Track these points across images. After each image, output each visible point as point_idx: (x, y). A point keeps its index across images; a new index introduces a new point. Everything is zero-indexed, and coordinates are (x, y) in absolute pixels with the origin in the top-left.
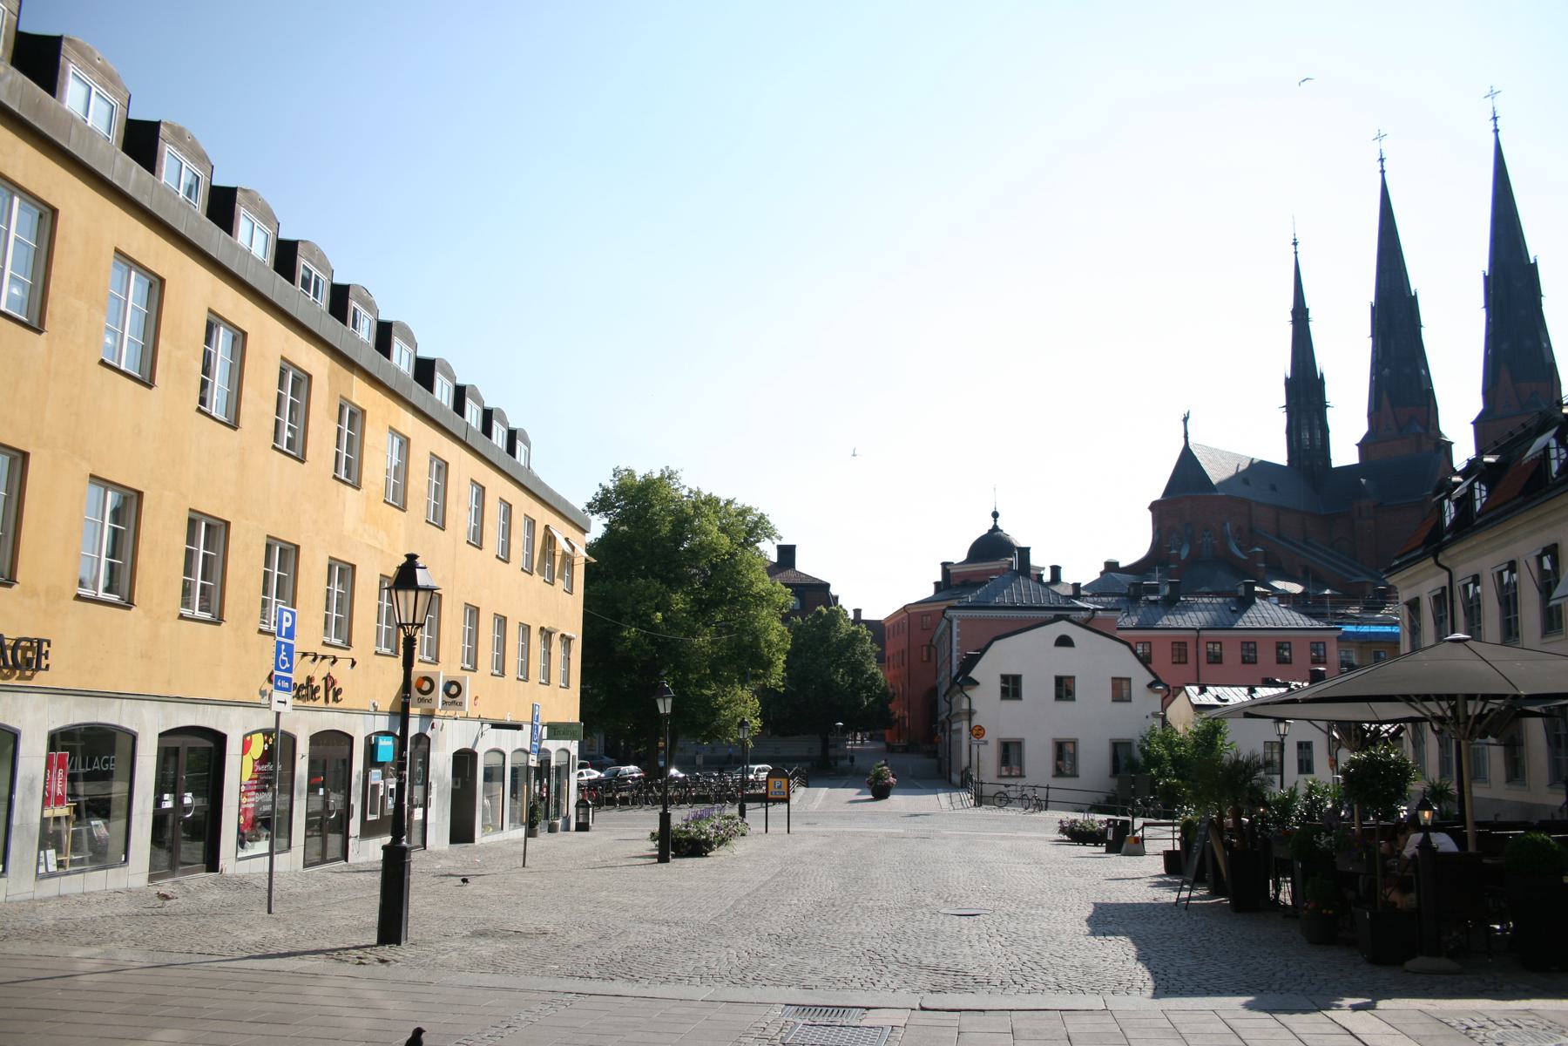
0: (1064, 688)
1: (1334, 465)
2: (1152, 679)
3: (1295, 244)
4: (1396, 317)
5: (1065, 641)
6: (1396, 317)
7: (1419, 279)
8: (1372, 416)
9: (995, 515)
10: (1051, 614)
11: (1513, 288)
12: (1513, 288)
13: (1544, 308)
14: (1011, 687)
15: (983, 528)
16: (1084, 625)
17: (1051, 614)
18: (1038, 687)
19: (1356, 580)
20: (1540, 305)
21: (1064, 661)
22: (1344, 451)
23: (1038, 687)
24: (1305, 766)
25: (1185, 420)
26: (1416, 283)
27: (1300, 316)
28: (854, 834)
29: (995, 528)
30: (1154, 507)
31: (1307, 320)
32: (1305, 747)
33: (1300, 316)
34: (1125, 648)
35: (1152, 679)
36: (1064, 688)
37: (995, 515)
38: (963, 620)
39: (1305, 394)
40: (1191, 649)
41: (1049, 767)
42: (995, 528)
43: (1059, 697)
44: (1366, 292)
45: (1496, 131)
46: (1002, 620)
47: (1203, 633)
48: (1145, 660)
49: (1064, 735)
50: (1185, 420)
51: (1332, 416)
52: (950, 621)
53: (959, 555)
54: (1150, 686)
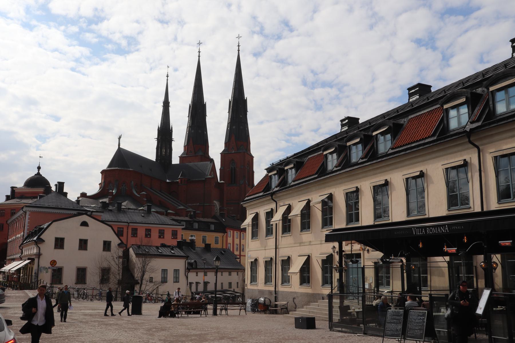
0: (83, 244)
1: (173, 163)
2: (120, 242)
3: (167, 76)
4: (198, 110)
5: (84, 224)
6: (198, 110)
7: (207, 98)
8: (226, 144)
9: (39, 168)
10: (75, 212)
11: (238, 106)
12: (238, 106)
13: (248, 116)
14: (59, 243)
15: (33, 173)
16: (90, 216)
17: (75, 212)
18: (71, 243)
19: (180, 208)
20: (247, 115)
21: (84, 233)
22: (175, 160)
23: (71, 243)
24: (176, 280)
25: (119, 138)
26: (246, 95)
27: (166, 104)
28: (101, 321)
29: (38, 174)
30: (103, 172)
31: (169, 106)
32: (176, 271)
33: (166, 104)
34: (110, 228)
35: (120, 242)
36: (83, 244)
37: (39, 168)
38: (32, 212)
39: (165, 134)
40: (125, 231)
41: (97, 279)
42: (38, 174)
43: (104, 250)
44: (229, 95)
45: (199, 56)
46: (59, 213)
47: (130, 224)
48: (119, 234)
49: (82, 265)
50: (119, 138)
51: (174, 144)
52: (25, 212)
53: (20, 184)
54: (119, 245)
